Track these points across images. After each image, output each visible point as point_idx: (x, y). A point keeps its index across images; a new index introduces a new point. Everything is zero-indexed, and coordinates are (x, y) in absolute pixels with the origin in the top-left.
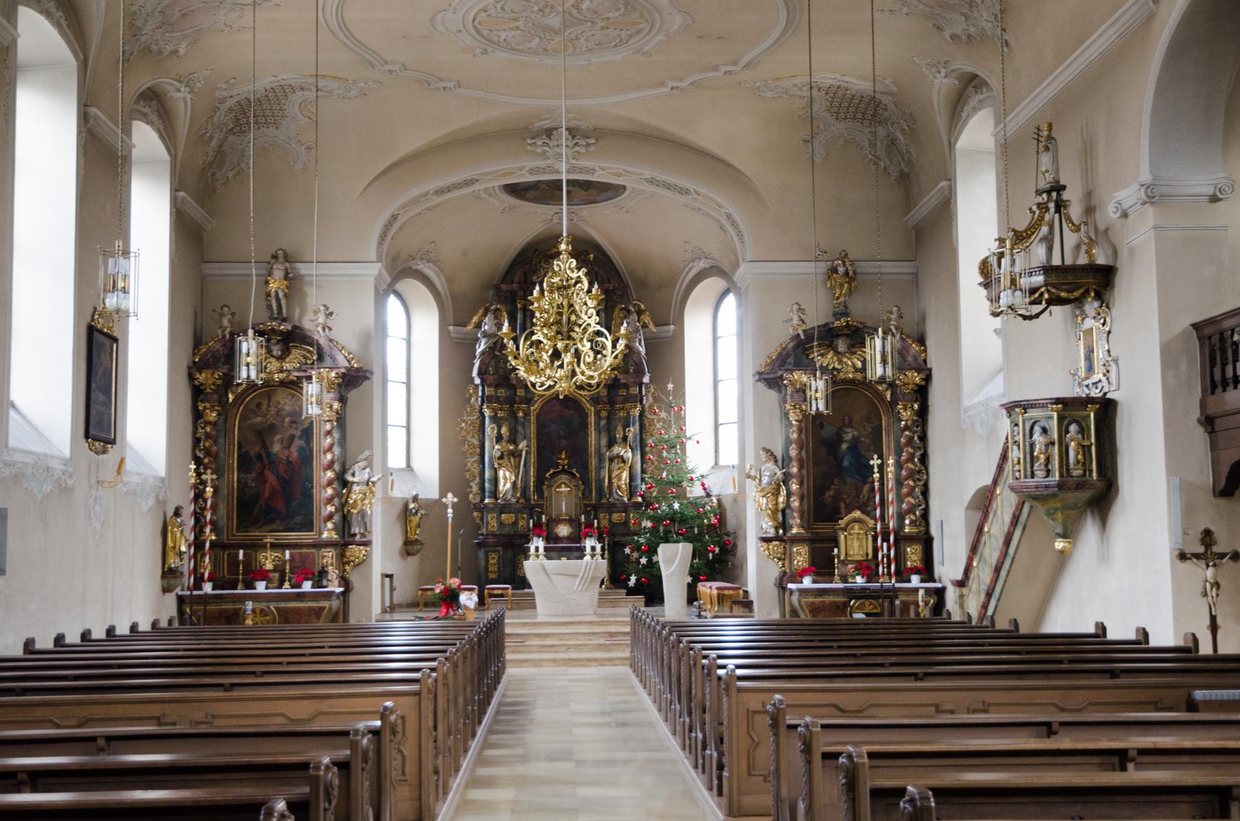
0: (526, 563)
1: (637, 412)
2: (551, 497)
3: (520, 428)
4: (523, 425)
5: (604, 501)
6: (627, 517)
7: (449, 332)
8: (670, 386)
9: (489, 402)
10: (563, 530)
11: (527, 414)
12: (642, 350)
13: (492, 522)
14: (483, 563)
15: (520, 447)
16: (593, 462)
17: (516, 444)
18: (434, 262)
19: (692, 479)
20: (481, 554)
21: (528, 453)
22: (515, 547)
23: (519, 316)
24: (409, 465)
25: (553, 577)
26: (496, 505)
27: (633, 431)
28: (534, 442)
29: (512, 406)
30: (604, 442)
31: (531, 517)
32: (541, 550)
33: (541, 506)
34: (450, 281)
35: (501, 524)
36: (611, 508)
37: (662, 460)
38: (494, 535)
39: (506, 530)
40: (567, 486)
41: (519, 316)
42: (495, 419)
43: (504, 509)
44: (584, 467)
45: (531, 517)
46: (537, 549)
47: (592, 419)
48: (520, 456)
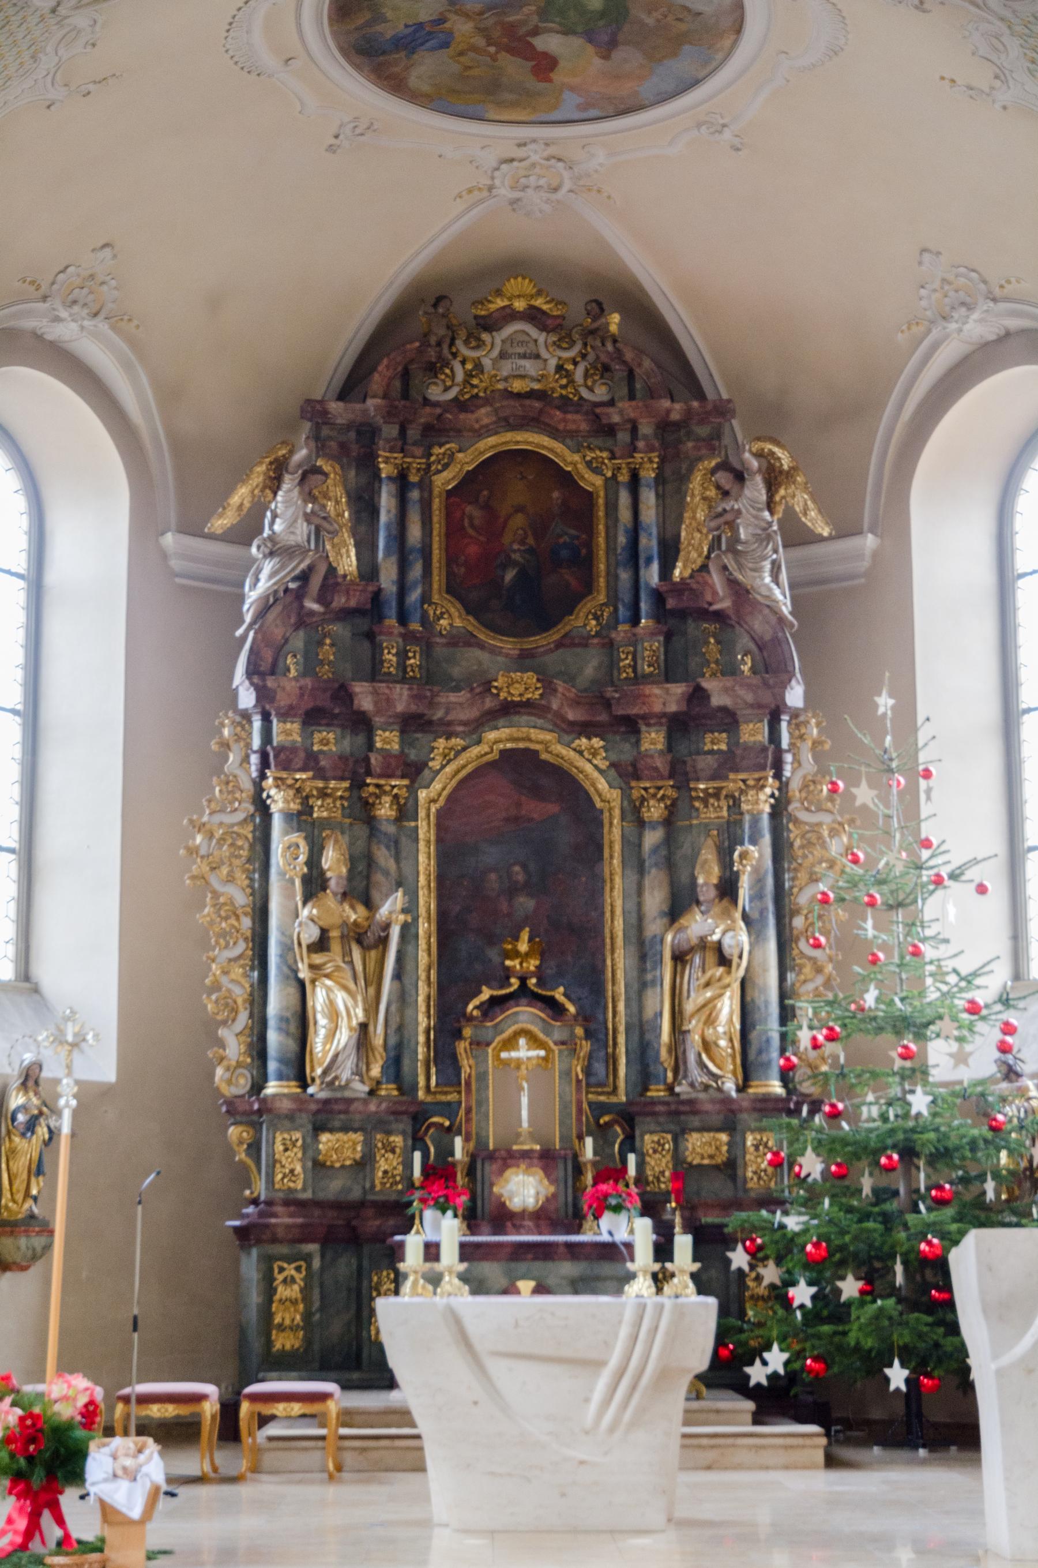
0: (383, 1305)
1: (763, 802)
2: (482, 1077)
3: (383, 856)
4: (395, 846)
5: (657, 1092)
6: (736, 1146)
7: (164, 556)
8: (885, 703)
9: (286, 766)
10: (523, 1189)
11: (405, 812)
12: (782, 599)
13: (288, 1163)
14: (254, 1298)
15: (384, 912)
16: (620, 962)
17: (369, 904)
18: (118, 320)
19: (974, 1008)
20: (250, 1266)
21: (408, 933)
22: (358, 1239)
23: (386, 501)
24: (25, 974)
25: (497, 1368)
26: (301, 1102)
27: (755, 856)
28: (427, 901)
29: (358, 784)
30: (655, 900)
31: (417, 1141)
32: (449, 1255)
33: (449, 1109)
34: (169, 395)
35: (318, 1166)
36: (680, 1116)
37: (851, 945)
38: (292, 1202)
39: (334, 1187)
40: (535, 1042)
41: (386, 501)
42: (301, 818)
43: (326, 1116)
44: (592, 983)
45: (417, 1141)
46: (432, 1251)
47: (614, 833)
48: (383, 942)
